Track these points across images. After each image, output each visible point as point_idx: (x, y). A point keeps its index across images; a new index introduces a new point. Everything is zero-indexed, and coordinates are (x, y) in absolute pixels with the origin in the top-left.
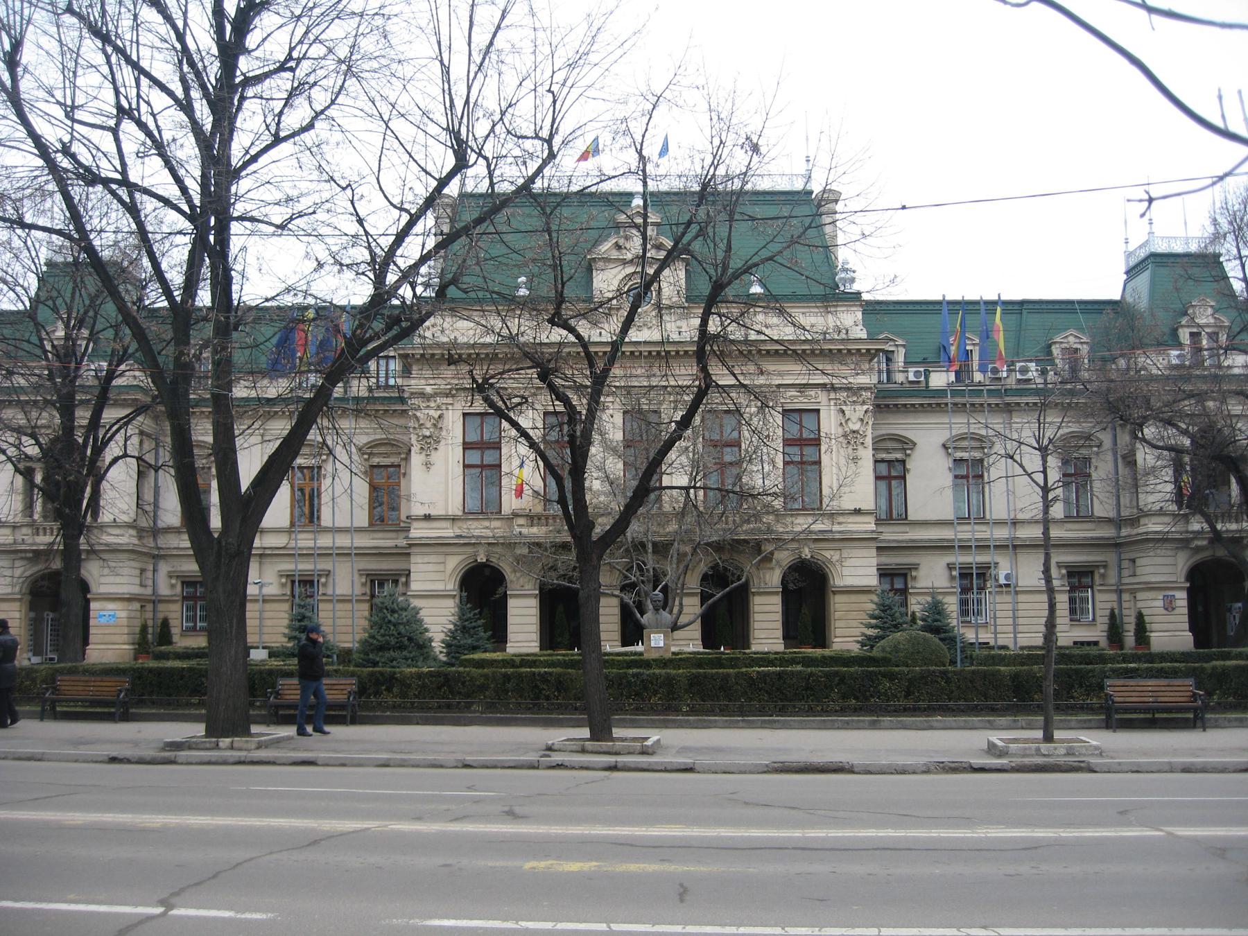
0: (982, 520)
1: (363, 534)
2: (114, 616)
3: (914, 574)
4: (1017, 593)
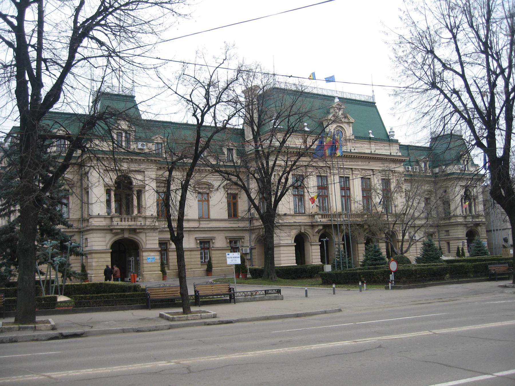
0: (208, 219)
1: (226, 222)
2: (154, 258)
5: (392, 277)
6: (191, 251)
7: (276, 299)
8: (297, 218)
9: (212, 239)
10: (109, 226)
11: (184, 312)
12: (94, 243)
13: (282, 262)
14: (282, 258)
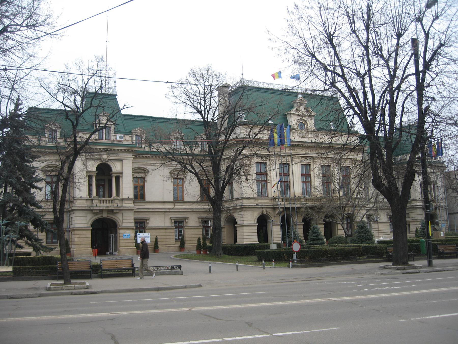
2: (129, 235)
3: (187, 221)
4: (378, 223)
5: (295, 257)
6: (166, 229)
7: (176, 274)
8: (260, 201)
9: (186, 219)
10: (90, 207)
11: (65, 284)
12: (76, 222)
13: (245, 240)
14: (245, 237)
